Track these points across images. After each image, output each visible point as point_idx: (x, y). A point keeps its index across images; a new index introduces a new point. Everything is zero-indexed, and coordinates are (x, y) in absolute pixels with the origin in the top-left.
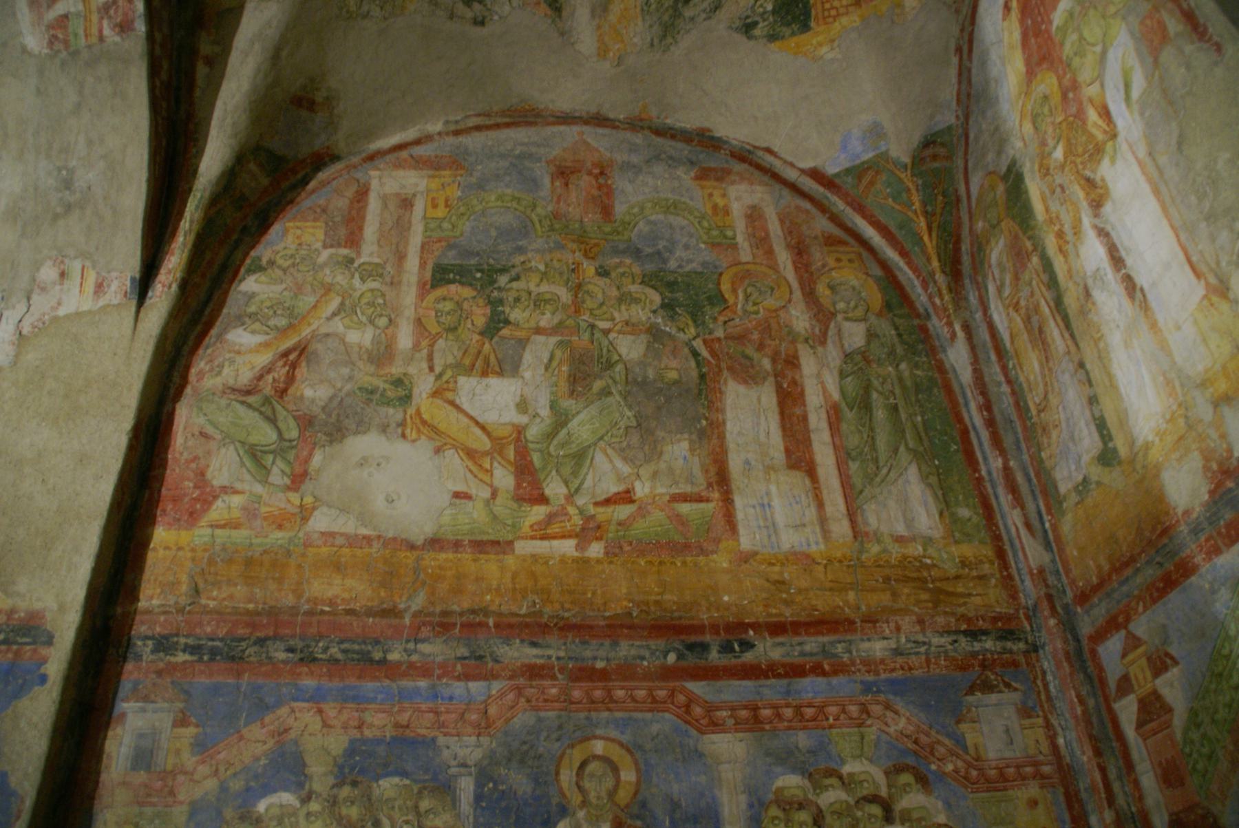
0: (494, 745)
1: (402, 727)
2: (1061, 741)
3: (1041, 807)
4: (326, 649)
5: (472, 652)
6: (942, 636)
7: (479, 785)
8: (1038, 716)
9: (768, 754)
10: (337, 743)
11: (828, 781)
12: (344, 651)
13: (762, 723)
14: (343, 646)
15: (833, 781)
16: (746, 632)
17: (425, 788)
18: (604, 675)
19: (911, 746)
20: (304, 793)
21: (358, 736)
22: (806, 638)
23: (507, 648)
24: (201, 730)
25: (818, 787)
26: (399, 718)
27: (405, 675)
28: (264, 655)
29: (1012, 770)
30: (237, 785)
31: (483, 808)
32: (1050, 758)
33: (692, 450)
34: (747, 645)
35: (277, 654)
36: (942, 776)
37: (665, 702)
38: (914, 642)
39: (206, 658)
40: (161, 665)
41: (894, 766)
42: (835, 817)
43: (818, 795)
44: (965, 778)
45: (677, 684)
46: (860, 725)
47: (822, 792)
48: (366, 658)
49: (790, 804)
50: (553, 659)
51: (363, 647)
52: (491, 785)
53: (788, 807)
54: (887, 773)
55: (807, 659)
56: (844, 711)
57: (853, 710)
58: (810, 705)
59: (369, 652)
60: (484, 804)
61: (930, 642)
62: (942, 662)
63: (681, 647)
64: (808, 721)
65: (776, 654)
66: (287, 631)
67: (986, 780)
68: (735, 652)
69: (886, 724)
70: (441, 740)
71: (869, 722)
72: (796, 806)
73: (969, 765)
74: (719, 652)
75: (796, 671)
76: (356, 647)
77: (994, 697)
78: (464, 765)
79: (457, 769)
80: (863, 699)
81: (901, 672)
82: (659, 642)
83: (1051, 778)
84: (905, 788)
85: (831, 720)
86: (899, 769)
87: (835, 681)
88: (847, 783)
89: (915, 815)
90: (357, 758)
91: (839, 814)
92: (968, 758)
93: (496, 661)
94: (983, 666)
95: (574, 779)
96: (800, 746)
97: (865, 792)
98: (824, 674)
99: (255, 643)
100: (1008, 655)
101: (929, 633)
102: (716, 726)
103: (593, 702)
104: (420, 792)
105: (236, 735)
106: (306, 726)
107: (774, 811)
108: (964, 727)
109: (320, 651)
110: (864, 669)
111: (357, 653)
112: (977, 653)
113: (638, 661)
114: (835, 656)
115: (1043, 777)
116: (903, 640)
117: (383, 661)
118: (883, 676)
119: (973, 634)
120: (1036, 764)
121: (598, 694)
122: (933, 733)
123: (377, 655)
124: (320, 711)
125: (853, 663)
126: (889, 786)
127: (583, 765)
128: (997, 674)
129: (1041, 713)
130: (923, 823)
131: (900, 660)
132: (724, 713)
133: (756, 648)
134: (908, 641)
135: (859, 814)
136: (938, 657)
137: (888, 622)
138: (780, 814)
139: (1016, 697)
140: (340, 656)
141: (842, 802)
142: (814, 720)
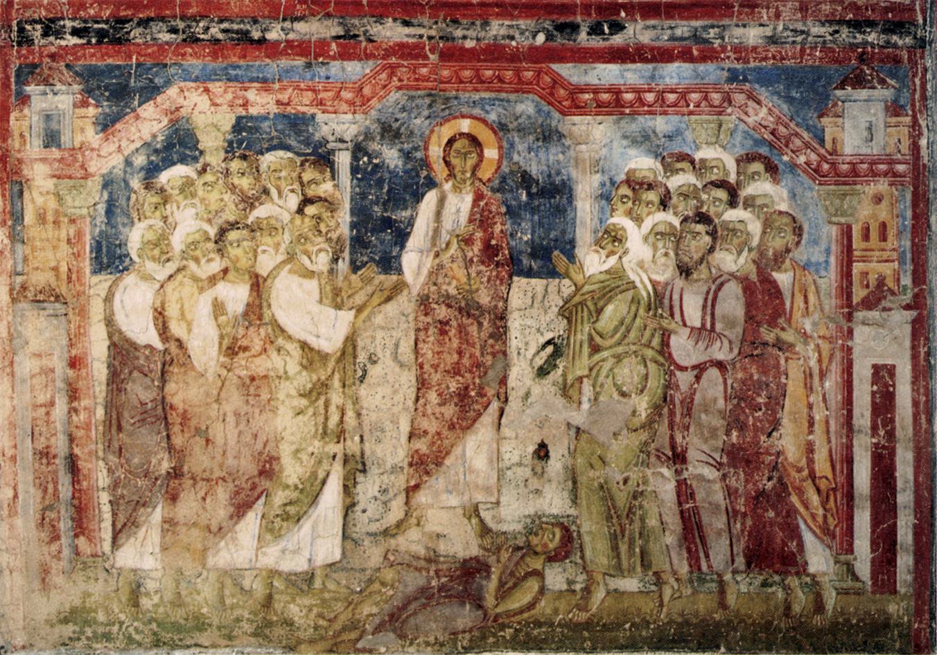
0: (368, 122)
1: (282, 104)
2: (923, 142)
3: (885, 203)
4: (207, 29)
5: (348, 31)
6: (823, 25)
7: (355, 158)
8: (907, 115)
9: (625, 137)
10: (227, 120)
11: (679, 165)
12: (225, 31)
13: (623, 107)
14: (225, 25)
15: (685, 165)
16: (619, 14)
17: (307, 161)
18: (472, 55)
19: (768, 136)
20: (199, 166)
21: (244, 113)
22: (678, 22)
23: (380, 27)
24: (100, 109)
25: (670, 170)
26: (280, 97)
27: (284, 53)
28: (149, 38)
29: (865, 166)
30: (140, 160)
31: (357, 179)
32: (908, 157)
33: (313, 134)
34: (617, 27)
35: (160, 36)
36: (793, 166)
37: (531, 83)
38: (792, 31)
39: (94, 41)
40: (53, 49)
41: (747, 155)
42: (682, 198)
43: (668, 177)
44: (816, 171)
45: (544, 65)
46: (720, 113)
47: (672, 175)
48: (244, 37)
49: (641, 184)
50: (425, 38)
51: (242, 26)
52: (365, 159)
53: (637, 187)
54: (738, 161)
55: (676, 43)
56: (706, 98)
57: (716, 97)
58: (673, 91)
59: (248, 32)
60: (359, 176)
61: (809, 30)
62: (818, 54)
63: (551, 28)
64: (668, 106)
65: (646, 38)
66: (167, 12)
67: (836, 174)
68: (605, 34)
69: (746, 113)
70: (320, 117)
71: (729, 110)
72: (646, 186)
73: (823, 158)
74: (589, 34)
75: (662, 55)
76: (235, 27)
77: (864, 93)
78: (342, 141)
79: (334, 144)
80: (726, 87)
81: (772, 61)
82: (529, 22)
83: (904, 176)
84: (753, 176)
85: (691, 107)
86: (749, 158)
87: (702, 67)
88: (699, 167)
89: (759, 202)
90: (244, 134)
91: (686, 196)
92: (823, 151)
93: (371, 41)
94: (862, 58)
95: (442, 155)
96: (658, 130)
97: (714, 178)
98: (691, 60)
99: (139, 24)
100: (890, 50)
101: (809, 23)
102: (578, 108)
103: (461, 82)
104: (302, 164)
105: (132, 114)
106: (195, 105)
107: (625, 190)
108: (825, 121)
109: (201, 31)
110: (733, 56)
111: (237, 32)
112: (857, 45)
113: (507, 41)
114: (706, 41)
115: (895, 175)
116: (780, 28)
117: (262, 41)
118: (752, 65)
119: (857, 25)
120: (891, 162)
121: (467, 73)
122: (792, 125)
123: (256, 35)
124: (207, 90)
125: (724, 49)
126: (738, 173)
127: (451, 142)
128: (873, 69)
129: (910, 113)
130: (765, 209)
131: (773, 49)
132: (587, 96)
133: (625, 31)
134: (786, 29)
135: (704, 197)
136: (814, 48)
137: (768, 8)
138: (629, 192)
139: (888, 94)
140: (220, 36)
141: (690, 185)
142: (675, 105)
